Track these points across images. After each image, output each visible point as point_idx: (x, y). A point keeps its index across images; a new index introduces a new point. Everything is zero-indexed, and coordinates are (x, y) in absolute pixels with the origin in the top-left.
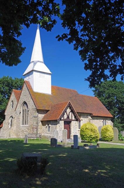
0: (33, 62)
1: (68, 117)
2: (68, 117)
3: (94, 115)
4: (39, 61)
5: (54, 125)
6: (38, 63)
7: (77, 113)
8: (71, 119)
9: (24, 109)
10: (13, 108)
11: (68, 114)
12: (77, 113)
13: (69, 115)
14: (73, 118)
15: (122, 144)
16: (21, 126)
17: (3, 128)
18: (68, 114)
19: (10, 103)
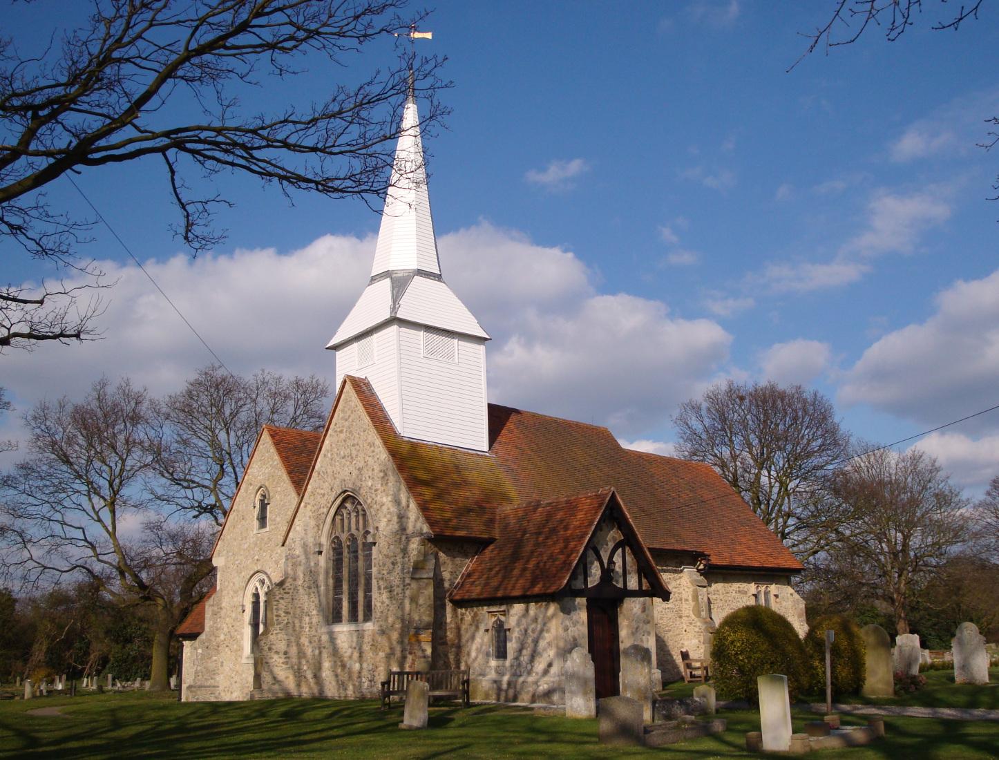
0: (387, 274)
1: (607, 573)
2: (607, 573)
3: (715, 560)
4: (420, 272)
5: (469, 575)
6: (418, 279)
7: (649, 549)
8: (620, 585)
9: (344, 537)
10: (262, 519)
11: (605, 562)
12: (649, 549)
13: (611, 562)
14: (633, 583)
15: (972, 732)
16: (110, 687)
17: (203, 637)
18: (605, 562)
19: (245, 505)
